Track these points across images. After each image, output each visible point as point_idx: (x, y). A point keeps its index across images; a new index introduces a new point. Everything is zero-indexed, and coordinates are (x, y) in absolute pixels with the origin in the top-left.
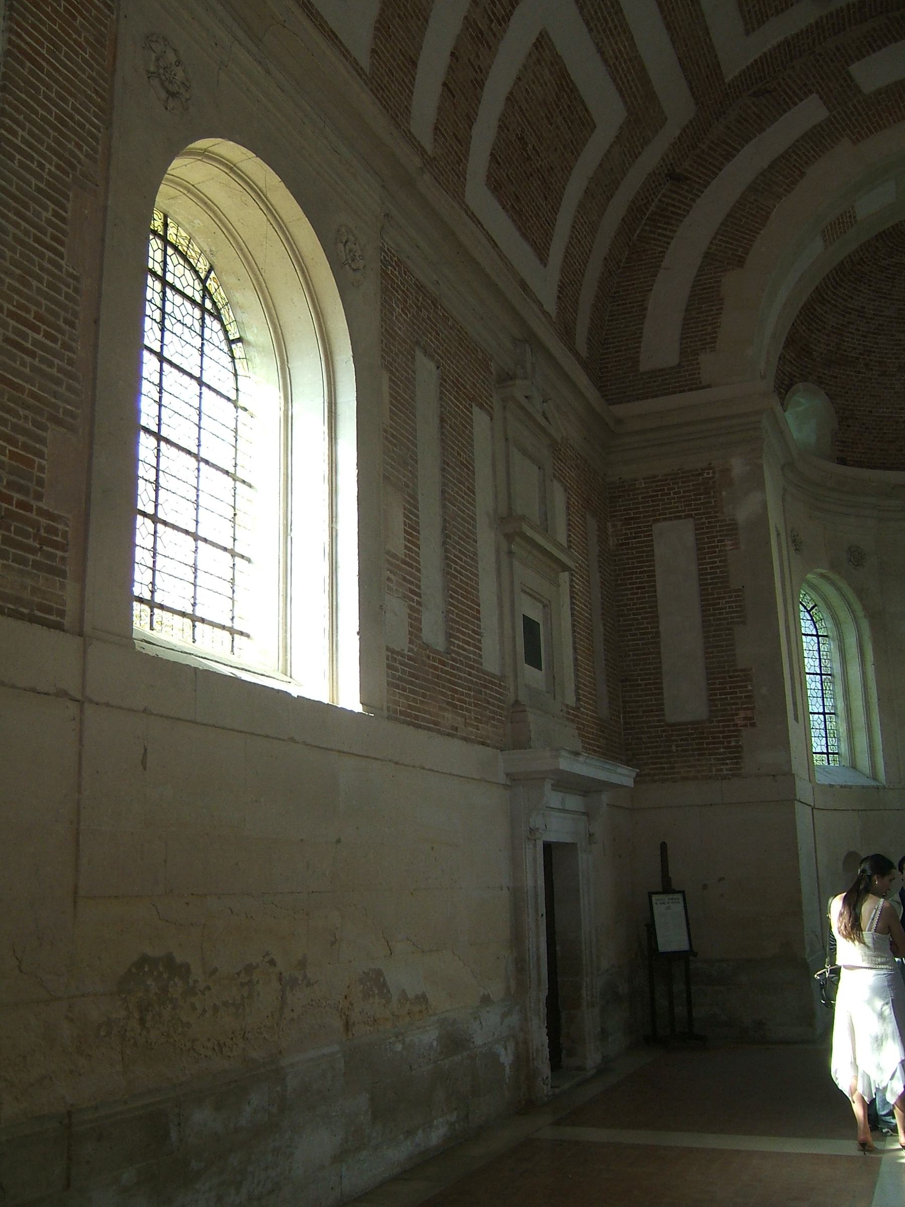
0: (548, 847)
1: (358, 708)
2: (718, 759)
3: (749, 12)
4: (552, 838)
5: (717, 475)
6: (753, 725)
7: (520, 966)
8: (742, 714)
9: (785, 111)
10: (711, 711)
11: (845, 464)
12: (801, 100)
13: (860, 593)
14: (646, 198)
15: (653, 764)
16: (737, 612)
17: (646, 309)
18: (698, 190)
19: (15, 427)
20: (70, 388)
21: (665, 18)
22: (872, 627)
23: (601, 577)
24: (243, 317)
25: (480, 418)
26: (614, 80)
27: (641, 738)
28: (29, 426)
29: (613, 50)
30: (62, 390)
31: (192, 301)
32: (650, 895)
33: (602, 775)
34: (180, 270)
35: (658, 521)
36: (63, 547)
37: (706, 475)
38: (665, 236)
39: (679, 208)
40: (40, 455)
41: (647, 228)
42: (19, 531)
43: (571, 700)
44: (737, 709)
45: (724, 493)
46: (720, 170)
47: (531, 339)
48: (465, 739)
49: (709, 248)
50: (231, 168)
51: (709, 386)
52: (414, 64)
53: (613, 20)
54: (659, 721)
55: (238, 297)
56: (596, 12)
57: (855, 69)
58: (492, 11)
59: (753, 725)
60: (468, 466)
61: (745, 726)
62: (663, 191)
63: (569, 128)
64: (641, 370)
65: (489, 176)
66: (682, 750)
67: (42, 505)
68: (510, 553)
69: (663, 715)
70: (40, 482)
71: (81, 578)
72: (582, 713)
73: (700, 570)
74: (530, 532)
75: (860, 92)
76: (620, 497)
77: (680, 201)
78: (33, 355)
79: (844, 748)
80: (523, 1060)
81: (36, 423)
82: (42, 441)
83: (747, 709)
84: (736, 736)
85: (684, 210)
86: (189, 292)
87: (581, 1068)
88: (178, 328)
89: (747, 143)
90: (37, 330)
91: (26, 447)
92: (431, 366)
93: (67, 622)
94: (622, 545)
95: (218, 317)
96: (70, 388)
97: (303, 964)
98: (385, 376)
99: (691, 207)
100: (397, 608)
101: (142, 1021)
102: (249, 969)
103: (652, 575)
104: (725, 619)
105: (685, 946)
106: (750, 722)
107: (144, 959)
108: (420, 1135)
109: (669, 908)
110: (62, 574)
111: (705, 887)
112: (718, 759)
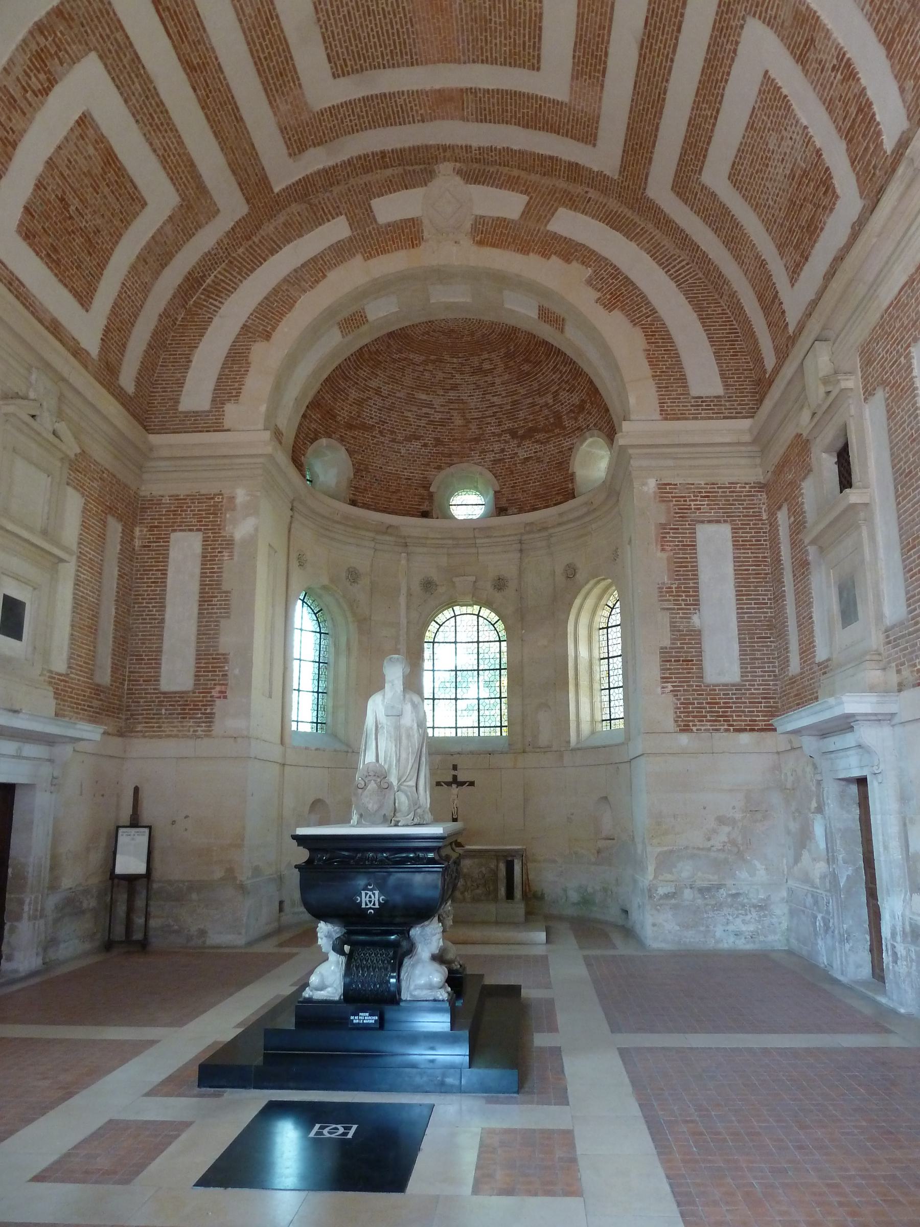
2: (196, 722)
3: (290, 139)
5: (225, 500)
6: (225, 697)
8: (218, 688)
9: (320, 225)
10: (195, 684)
11: (355, 505)
12: (333, 218)
14: (202, 271)
15: (146, 723)
16: (224, 609)
17: (191, 361)
18: (246, 274)
21: (212, 127)
23: (119, 571)
26: (165, 168)
27: (139, 702)
29: (161, 143)
32: (118, 827)
35: (175, 531)
37: (216, 500)
38: (215, 306)
39: (229, 285)
41: (203, 297)
44: (215, 685)
45: (228, 516)
46: (265, 261)
49: (247, 321)
51: (228, 430)
53: (158, 117)
54: (154, 689)
56: (142, 109)
57: (376, 203)
58: (27, 83)
59: (225, 697)
61: (220, 697)
62: (219, 269)
63: (118, 200)
64: (180, 410)
65: (21, 224)
66: (170, 714)
69: (159, 685)
72: (73, 679)
73: (202, 573)
75: (376, 221)
76: (149, 508)
77: (230, 280)
83: (223, 684)
84: (211, 705)
85: (233, 287)
89: (289, 243)
94: (145, 546)
99: (238, 286)
104: (216, 613)
106: (223, 695)
109: (133, 839)
111: (174, 822)
112: (196, 722)
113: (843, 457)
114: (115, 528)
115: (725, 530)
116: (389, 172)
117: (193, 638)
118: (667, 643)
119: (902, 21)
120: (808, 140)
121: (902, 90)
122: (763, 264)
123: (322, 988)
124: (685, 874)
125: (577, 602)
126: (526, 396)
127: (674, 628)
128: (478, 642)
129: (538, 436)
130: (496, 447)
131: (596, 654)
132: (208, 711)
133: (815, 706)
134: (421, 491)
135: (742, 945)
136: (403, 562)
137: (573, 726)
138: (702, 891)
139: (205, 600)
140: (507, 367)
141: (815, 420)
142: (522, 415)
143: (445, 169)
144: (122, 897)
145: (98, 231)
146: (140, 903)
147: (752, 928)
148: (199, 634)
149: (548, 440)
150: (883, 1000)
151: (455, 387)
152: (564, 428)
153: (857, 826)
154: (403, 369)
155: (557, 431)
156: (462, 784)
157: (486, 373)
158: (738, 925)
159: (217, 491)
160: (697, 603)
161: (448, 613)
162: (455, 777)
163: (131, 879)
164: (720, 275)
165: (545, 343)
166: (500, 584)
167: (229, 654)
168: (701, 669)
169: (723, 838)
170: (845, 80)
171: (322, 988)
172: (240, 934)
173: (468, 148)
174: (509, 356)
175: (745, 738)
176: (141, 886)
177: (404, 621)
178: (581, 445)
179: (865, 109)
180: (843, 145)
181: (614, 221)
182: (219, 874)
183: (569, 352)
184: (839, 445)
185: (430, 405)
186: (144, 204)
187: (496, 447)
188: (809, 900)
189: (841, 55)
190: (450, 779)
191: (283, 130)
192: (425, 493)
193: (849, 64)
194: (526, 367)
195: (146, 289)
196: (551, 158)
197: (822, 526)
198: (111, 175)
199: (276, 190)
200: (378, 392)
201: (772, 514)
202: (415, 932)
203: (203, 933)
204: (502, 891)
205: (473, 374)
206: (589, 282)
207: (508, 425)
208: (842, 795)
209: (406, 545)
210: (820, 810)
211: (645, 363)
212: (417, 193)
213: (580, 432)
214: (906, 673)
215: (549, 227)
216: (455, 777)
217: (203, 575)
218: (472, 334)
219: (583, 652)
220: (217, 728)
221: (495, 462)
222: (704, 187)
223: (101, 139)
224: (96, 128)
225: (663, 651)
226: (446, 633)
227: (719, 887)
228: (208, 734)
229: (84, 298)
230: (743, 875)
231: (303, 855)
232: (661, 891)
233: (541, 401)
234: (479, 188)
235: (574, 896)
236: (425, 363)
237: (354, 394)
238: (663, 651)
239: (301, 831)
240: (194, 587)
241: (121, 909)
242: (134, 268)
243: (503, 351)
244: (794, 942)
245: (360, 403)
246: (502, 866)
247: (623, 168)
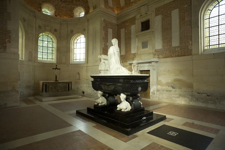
6: (10, 42)
8: (7, 39)
59: (10, 42)
61: (8, 42)
125: (73, 37)
127: (105, 45)
128: (219, 35)
132: (4, 45)
134: (38, 5)
136: (35, 20)
141: (141, 17)
149: (69, 4)
150: (150, 100)
155: (71, 3)
156: (58, 69)
162: (56, 68)
167: (11, 31)
172: (18, 103)
178: (77, 8)
190: (55, 68)
192: (39, 6)
204: (67, 89)
216: (56, 68)
221: (56, 5)
231: (92, 79)
246: (67, 85)
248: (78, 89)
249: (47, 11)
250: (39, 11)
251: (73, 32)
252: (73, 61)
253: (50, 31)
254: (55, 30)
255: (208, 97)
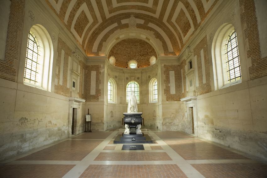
0: (74, 109)
1: (50, 91)
4: (74, 107)
7: (69, 122)
13: (116, 81)
19: (10, 59)
20: (17, 55)
22: (117, 85)
24: (40, 43)
25: (70, 57)
28: (12, 59)
30: (16, 55)
31: (33, 41)
33: (81, 101)
34: (31, 37)
36: (15, 73)
40: (13, 62)
42: (10, 71)
43: (79, 92)
47: (77, 48)
48: (64, 96)
50: (39, 27)
52: (65, 13)
55: (39, 41)
57: (121, 21)
60: (67, 63)
65: (74, 27)
67: (13, 68)
68: (72, 74)
70: (13, 65)
71: (17, 76)
74: (74, 72)
78: (13, 51)
79: (112, 99)
80: (68, 132)
81: (13, 59)
82: (13, 61)
86: (32, 40)
87: (76, 134)
88: (31, 44)
90: (13, 48)
91: (11, 61)
92: (64, 51)
93: (15, 81)
95: (36, 43)
96: (17, 55)
97: (41, 119)
98: (58, 53)
100: (56, 80)
101: (22, 124)
102: (35, 119)
103: (90, 77)
105: (90, 121)
107: (22, 118)
108: (54, 140)
110: (15, 76)
113: (191, 63)
114: (84, 70)
115: (173, 72)
116: (124, 16)
117: (95, 87)
118: (165, 88)
119: (201, 7)
120: (187, 19)
121: (200, 16)
122: (180, 34)
123: (126, 133)
124: (167, 121)
126: (143, 50)
127: (166, 86)
129: (144, 56)
130: (138, 57)
131: (153, 90)
133: (186, 98)
135: (175, 130)
137: (150, 101)
138: (170, 123)
139: (97, 81)
140: (140, 45)
142: (142, 52)
143: (132, 16)
144: (87, 125)
145: (83, 27)
146: (89, 125)
147: (176, 128)
148: (96, 86)
150: (194, 135)
151: (132, 48)
152: (149, 55)
153: (191, 113)
154: (124, 45)
157: (137, 46)
158: (174, 128)
159: (98, 65)
160: (169, 83)
161: (130, 83)
163: (88, 122)
164: (173, 34)
165: (146, 42)
166: (138, 78)
168: (170, 92)
169: (172, 116)
170: (193, 12)
171: (126, 133)
173: (136, 13)
174: (141, 43)
175: (176, 102)
176: (89, 123)
177: (123, 84)
179: (195, 17)
180: (192, 21)
181: (157, 25)
182: (100, 121)
183: (150, 44)
184: (190, 61)
185: (128, 51)
186: (89, 22)
187: (138, 57)
188: (184, 124)
189: (192, 9)
191: (109, 10)
193: (193, 10)
194: (143, 45)
195: (88, 34)
196: (149, 15)
197: (188, 73)
198: (85, 19)
199: (107, 19)
200: (120, 48)
201: (180, 70)
202: (138, 126)
203: (98, 130)
205: (135, 46)
206: (154, 34)
207: (139, 54)
208: (189, 110)
209: (124, 72)
210: (186, 112)
211: (162, 47)
212: (128, 19)
213: (151, 56)
214: (198, 93)
215: (148, 25)
217: (96, 78)
218: (135, 40)
219: (151, 89)
220: (99, 100)
222: (172, 22)
223: (85, 14)
224: (84, 12)
225: (164, 89)
226: (130, 86)
227: (172, 123)
228: (98, 101)
229: (81, 37)
230: (175, 121)
232: (164, 123)
233: (145, 50)
234: (138, 19)
235: (150, 125)
236: (127, 44)
237: (116, 49)
238: (164, 89)
239: (124, 113)
240: (95, 79)
241: (87, 127)
242: (86, 31)
243: (139, 43)
244: (182, 130)
245: (117, 50)
247: (159, 17)
248: (154, 124)
249: (133, 65)
250: (126, 67)
251: (150, 77)
252: (152, 101)
253: (135, 80)
254: (138, 78)
255: (220, 133)
